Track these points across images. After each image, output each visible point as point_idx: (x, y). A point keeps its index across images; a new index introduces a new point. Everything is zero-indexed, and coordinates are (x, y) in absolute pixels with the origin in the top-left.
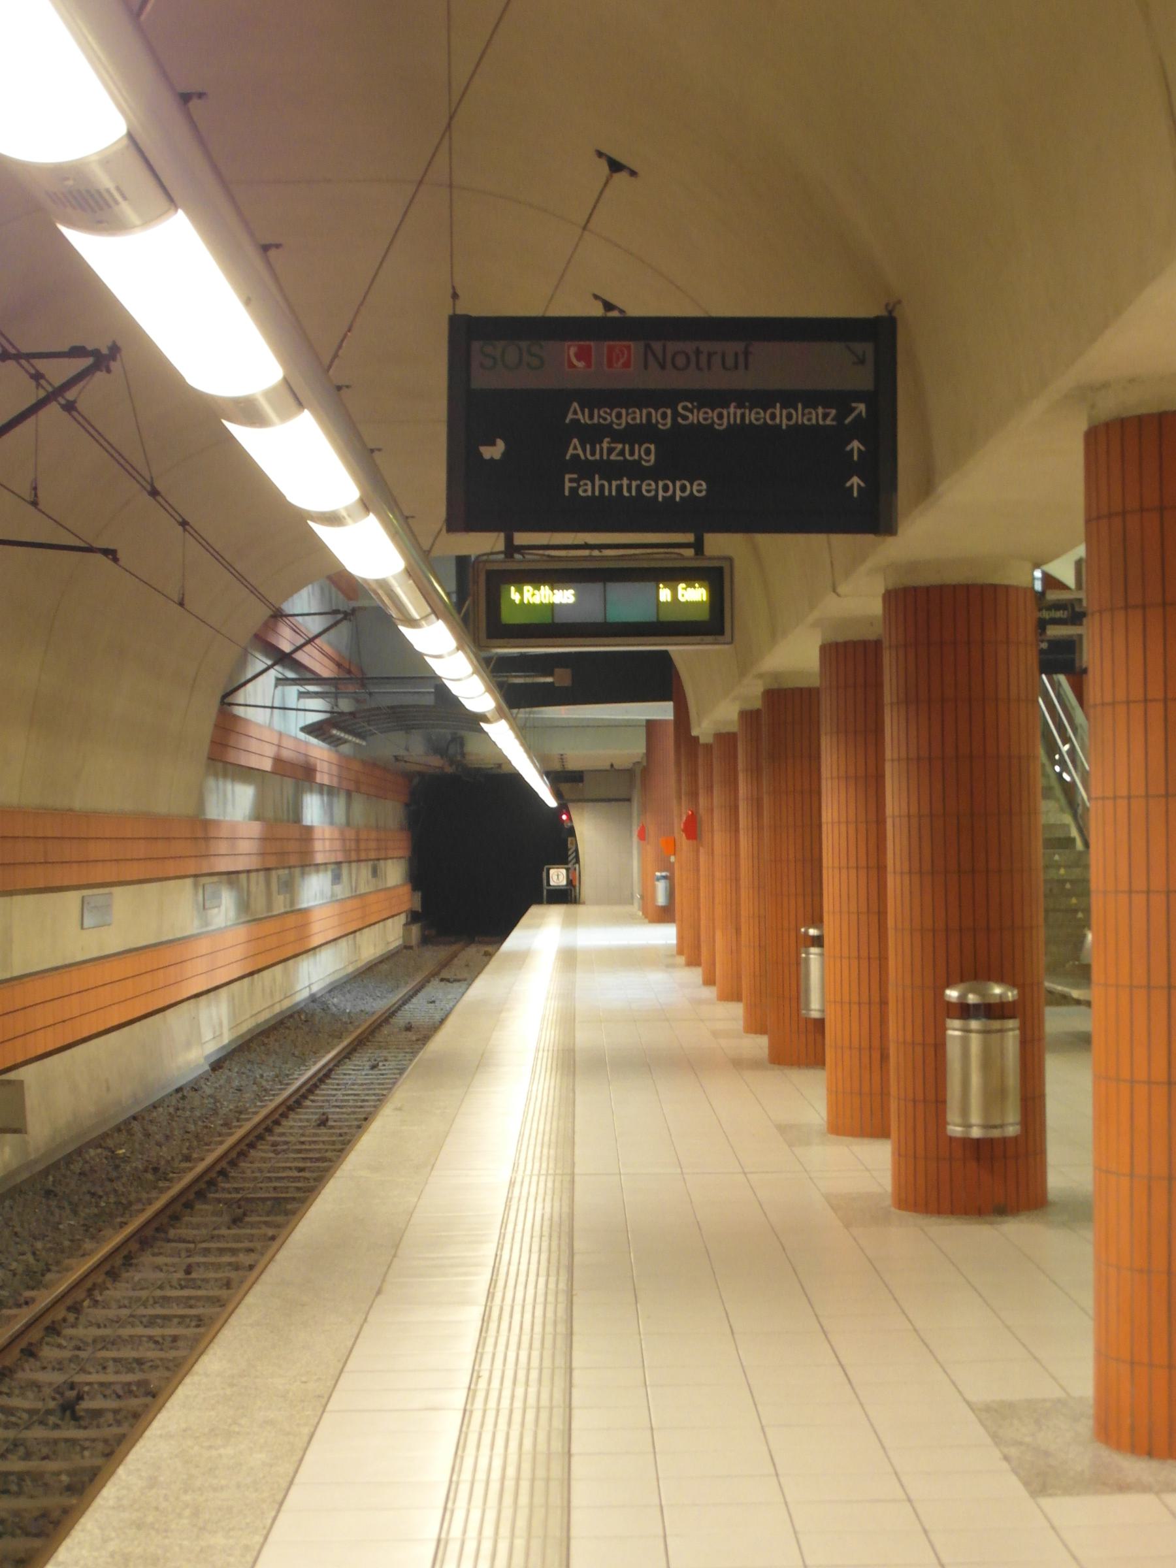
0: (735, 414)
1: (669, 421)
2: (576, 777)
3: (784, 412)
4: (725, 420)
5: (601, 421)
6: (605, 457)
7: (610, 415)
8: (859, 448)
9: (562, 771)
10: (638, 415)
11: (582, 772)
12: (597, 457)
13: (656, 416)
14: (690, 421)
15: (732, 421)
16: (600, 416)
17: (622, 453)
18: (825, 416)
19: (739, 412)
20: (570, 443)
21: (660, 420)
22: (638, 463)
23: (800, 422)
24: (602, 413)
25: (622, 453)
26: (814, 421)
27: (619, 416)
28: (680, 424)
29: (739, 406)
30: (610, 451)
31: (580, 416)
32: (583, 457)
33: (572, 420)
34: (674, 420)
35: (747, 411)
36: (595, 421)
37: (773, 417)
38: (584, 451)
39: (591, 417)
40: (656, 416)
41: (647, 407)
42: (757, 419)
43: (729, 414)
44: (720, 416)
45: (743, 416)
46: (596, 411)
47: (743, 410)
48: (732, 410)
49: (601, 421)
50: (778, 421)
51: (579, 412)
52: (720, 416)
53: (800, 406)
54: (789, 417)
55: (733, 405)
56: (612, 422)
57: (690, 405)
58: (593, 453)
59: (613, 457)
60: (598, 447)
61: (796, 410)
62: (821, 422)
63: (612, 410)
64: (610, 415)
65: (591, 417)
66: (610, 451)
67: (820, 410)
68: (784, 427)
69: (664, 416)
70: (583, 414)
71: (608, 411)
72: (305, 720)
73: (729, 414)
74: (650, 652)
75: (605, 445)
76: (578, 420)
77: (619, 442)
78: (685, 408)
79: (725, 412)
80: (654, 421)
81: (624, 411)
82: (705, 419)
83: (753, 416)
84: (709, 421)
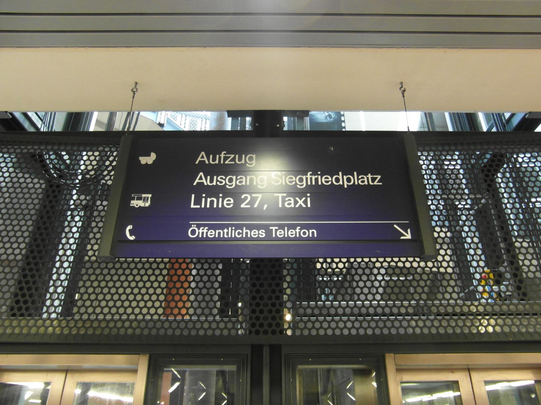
0: (311, 179)
3: (345, 177)
4: (304, 182)
5: (218, 183)
6: (222, 162)
7: (225, 180)
8: (405, 236)
10: (244, 180)
12: (217, 162)
15: (309, 183)
16: (217, 181)
17: (233, 159)
18: (373, 180)
19: (314, 177)
21: (258, 182)
23: (356, 183)
24: (219, 179)
25: (233, 159)
26: (366, 183)
27: (231, 180)
30: (226, 159)
31: (204, 181)
32: (207, 162)
35: (319, 177)
36: (214, 183)
37: (337, 180)
38: (208, 159)
39: (211, 181)
42: (327, 182)
43: (307, 179)
45: (317, 180)
46: (215, 177)
47: (316, 176)
48: (309, 176)
49: (218, 183)
50: (341, 183)
54: (349, 180)
56: (226, 184)
58: (214, 160)
60: (218, 156)
62: (371, 183)
63: (226, 178)
64: (225, 180)
65: (211, 181)
66: (226, 159)
67: (370, 176)
71: (224, 177)
73: (307, 179)
75: (222, 155)
76: (203, 183)
77: (233, 154)
79: (304, 177)
81: (234, 178)
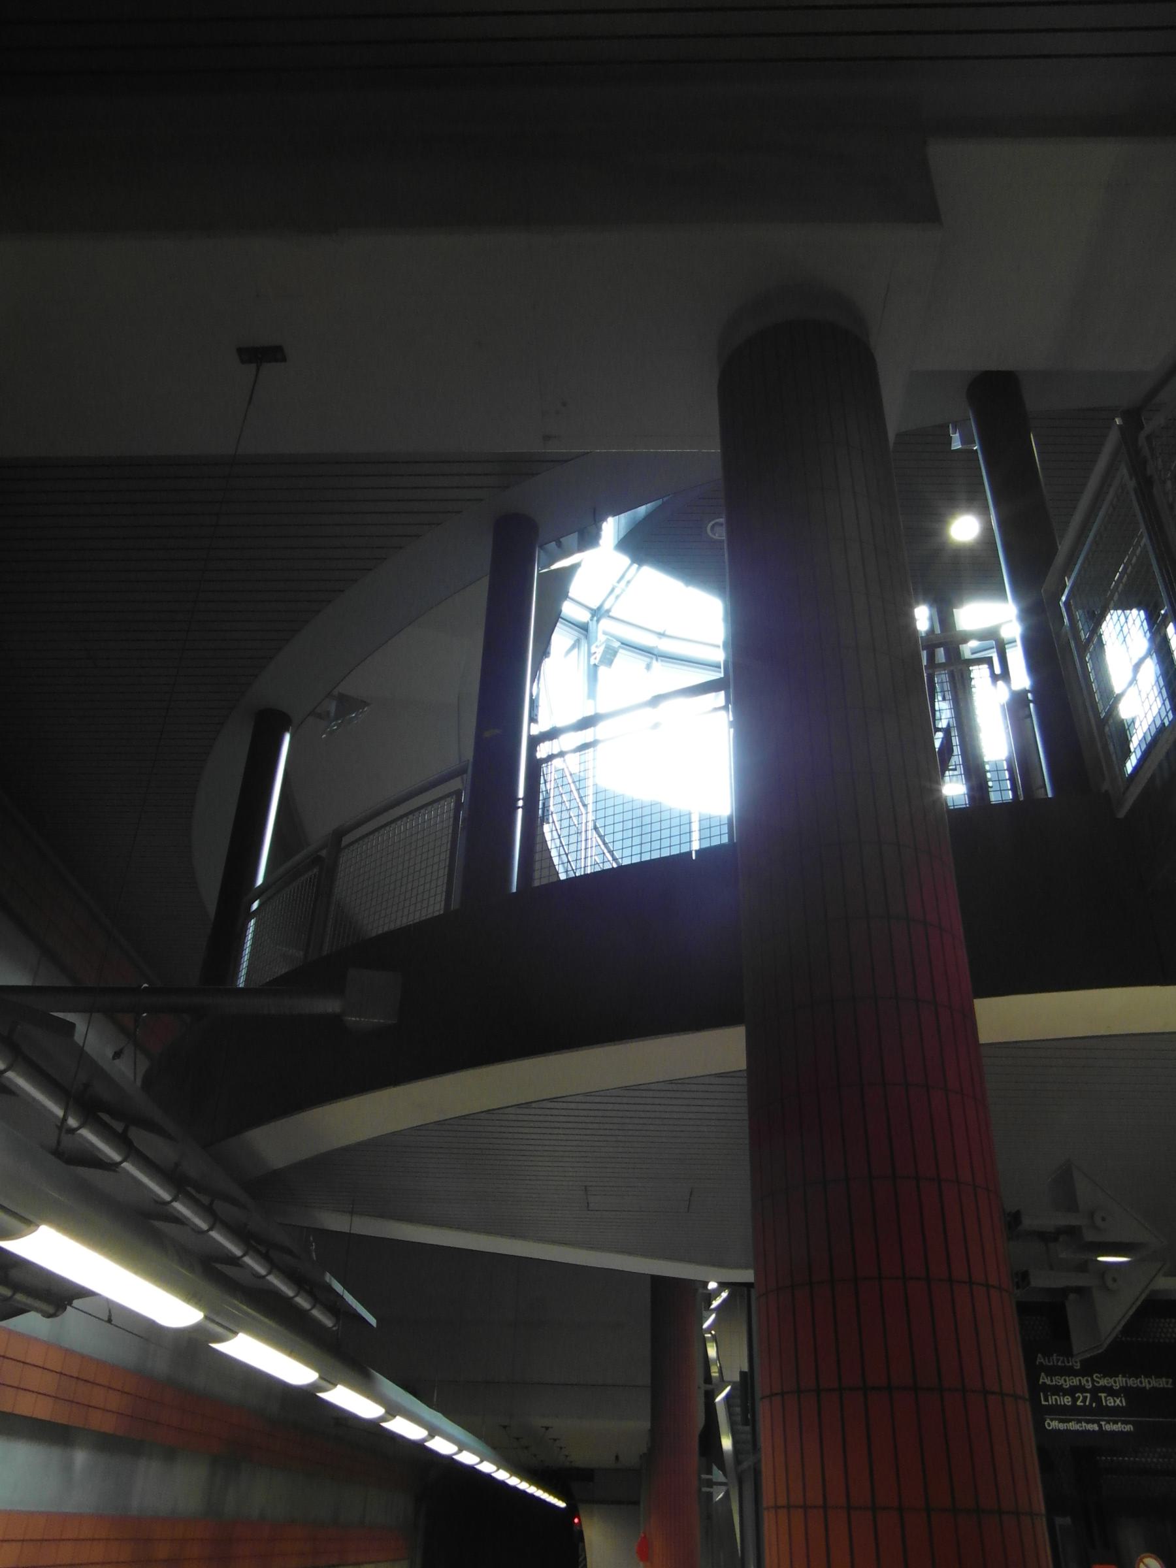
1: (1090, 1383)
2: (586, 1475)
9: (567, 879)
11: (592, 1470)
13: (1084, 1381)
14: (1100, 1384)
16: (1056, 1381)
17: (1063, 1362)
18: (1167, 1383)
19: (1124, 1379)
20: (1040, 1376)
22: (1072, 1367)
27: (1065, 1381)
28: (1096, 1386)
29: (1123, 1376)
31: (1046, 1381)
33: (1042, 1382)
34: (1093, 1384)
36: (1054, 1383)
37: (1141, 1382)
39: (1052, 1381)
40: (1084, 1381)
41: (1078, 1376)
43: (1119, 1380)
44: (1115, 1382)
51: (1045, 1378)
52: (1115, 1382)
53: (1153, 1377)
55: (1120, 1376)
57: (1099, 1376)
58: (1049, 1362)
59: (1059, 1364)
60: (1051, 1358)
61: (1152, 1378)
68: (1148, 1388)
69: (1087, 1381)
70: (1045, 1359)
72: (595, 731)
74: (1033, 449)
75: (1055, 1357)
78: (1097, 1377)
80: (1083, 1384)
82: (1108, 1383)
83: (1131, 1382)
84: (1110, 1385)
